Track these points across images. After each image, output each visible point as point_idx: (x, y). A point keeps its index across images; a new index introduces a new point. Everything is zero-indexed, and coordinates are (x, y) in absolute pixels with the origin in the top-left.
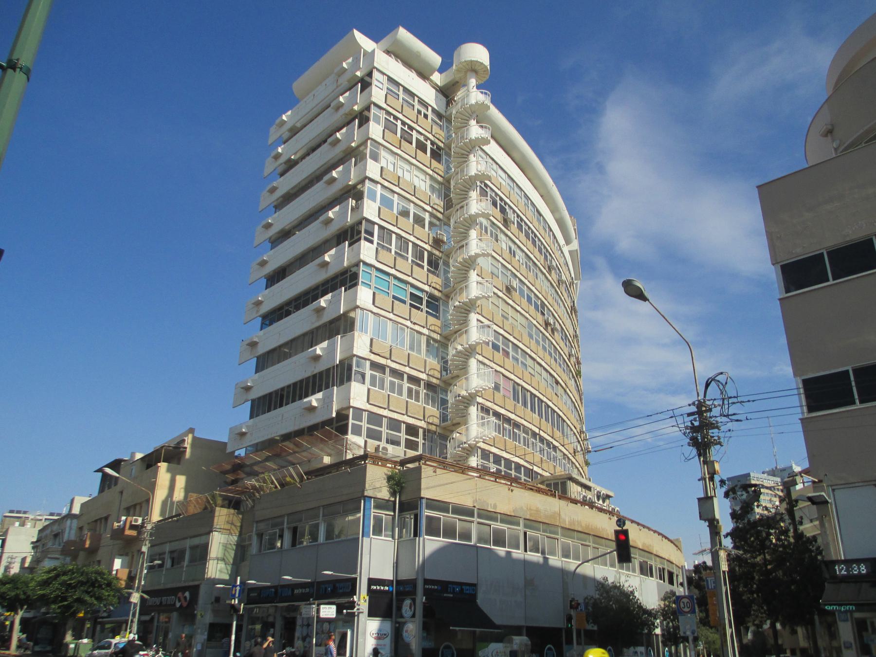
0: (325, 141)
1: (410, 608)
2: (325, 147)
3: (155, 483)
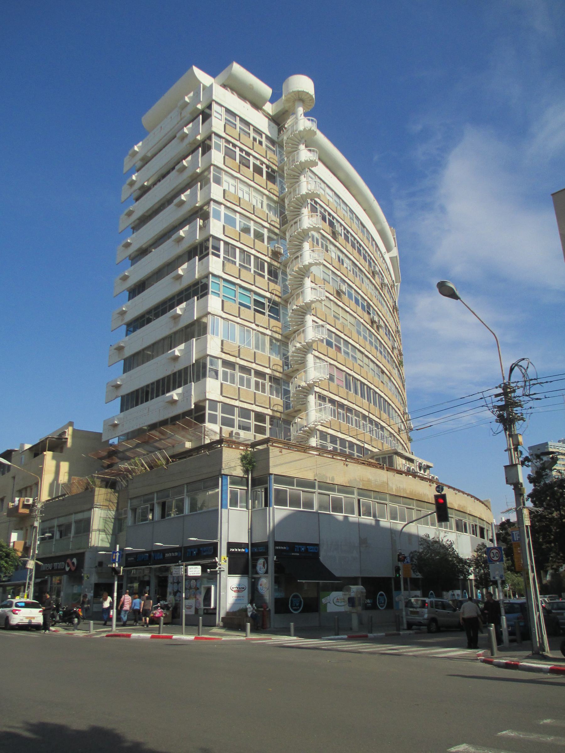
1: (264, 566)
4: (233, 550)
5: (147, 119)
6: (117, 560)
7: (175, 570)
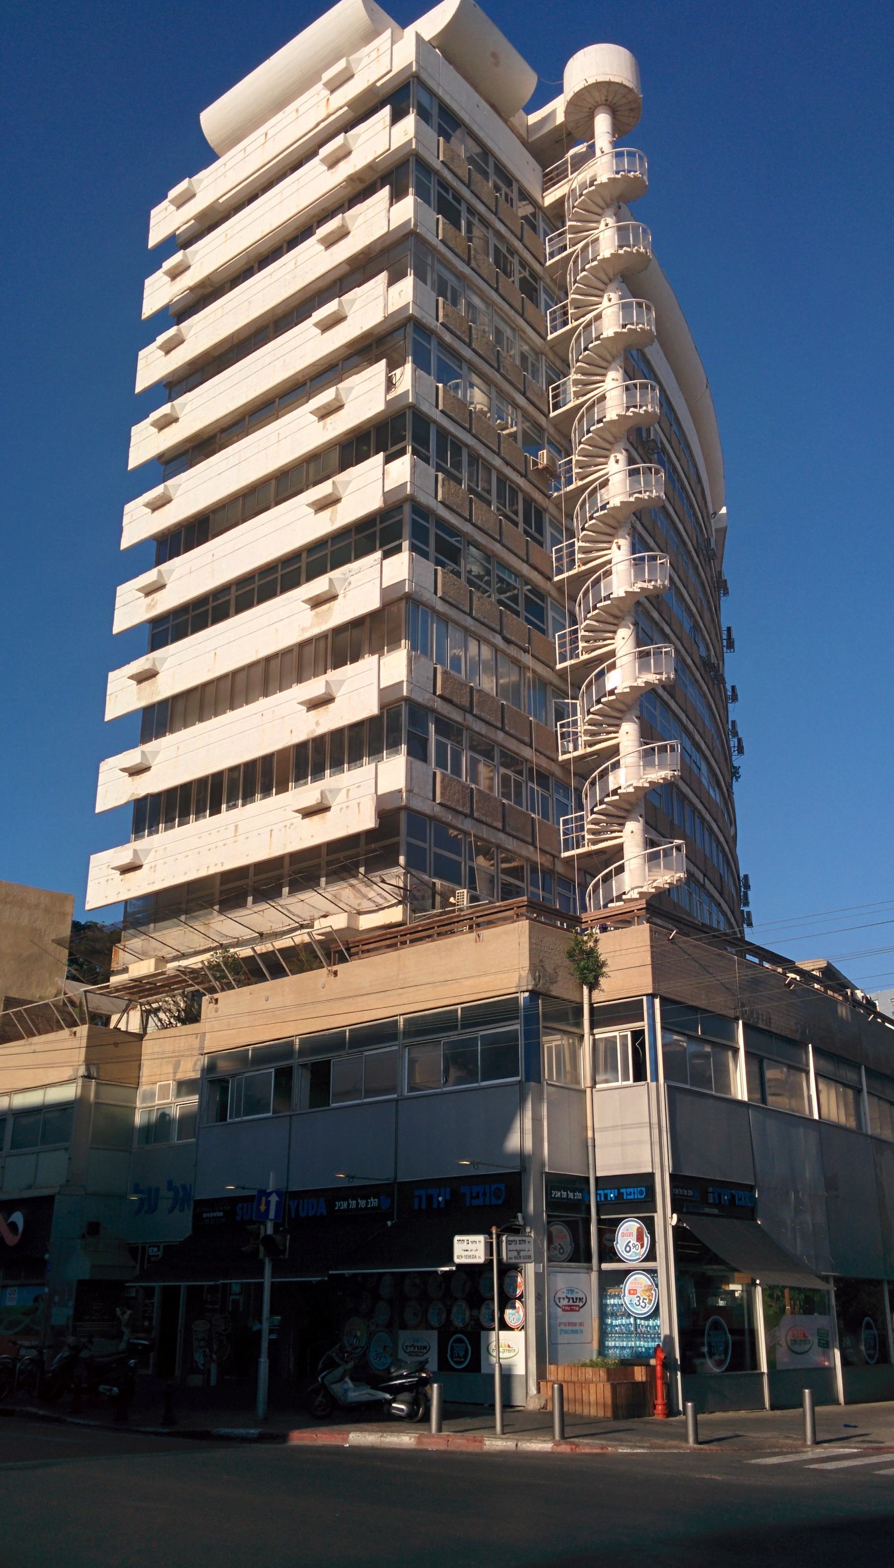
0: (314, 153)
1: (640, 1238)
2: (314, 166)
3: (562, 84)
4: (345, 1205)
5: (213, 119)
6: (272, 1215)
7: (464, 1246)
